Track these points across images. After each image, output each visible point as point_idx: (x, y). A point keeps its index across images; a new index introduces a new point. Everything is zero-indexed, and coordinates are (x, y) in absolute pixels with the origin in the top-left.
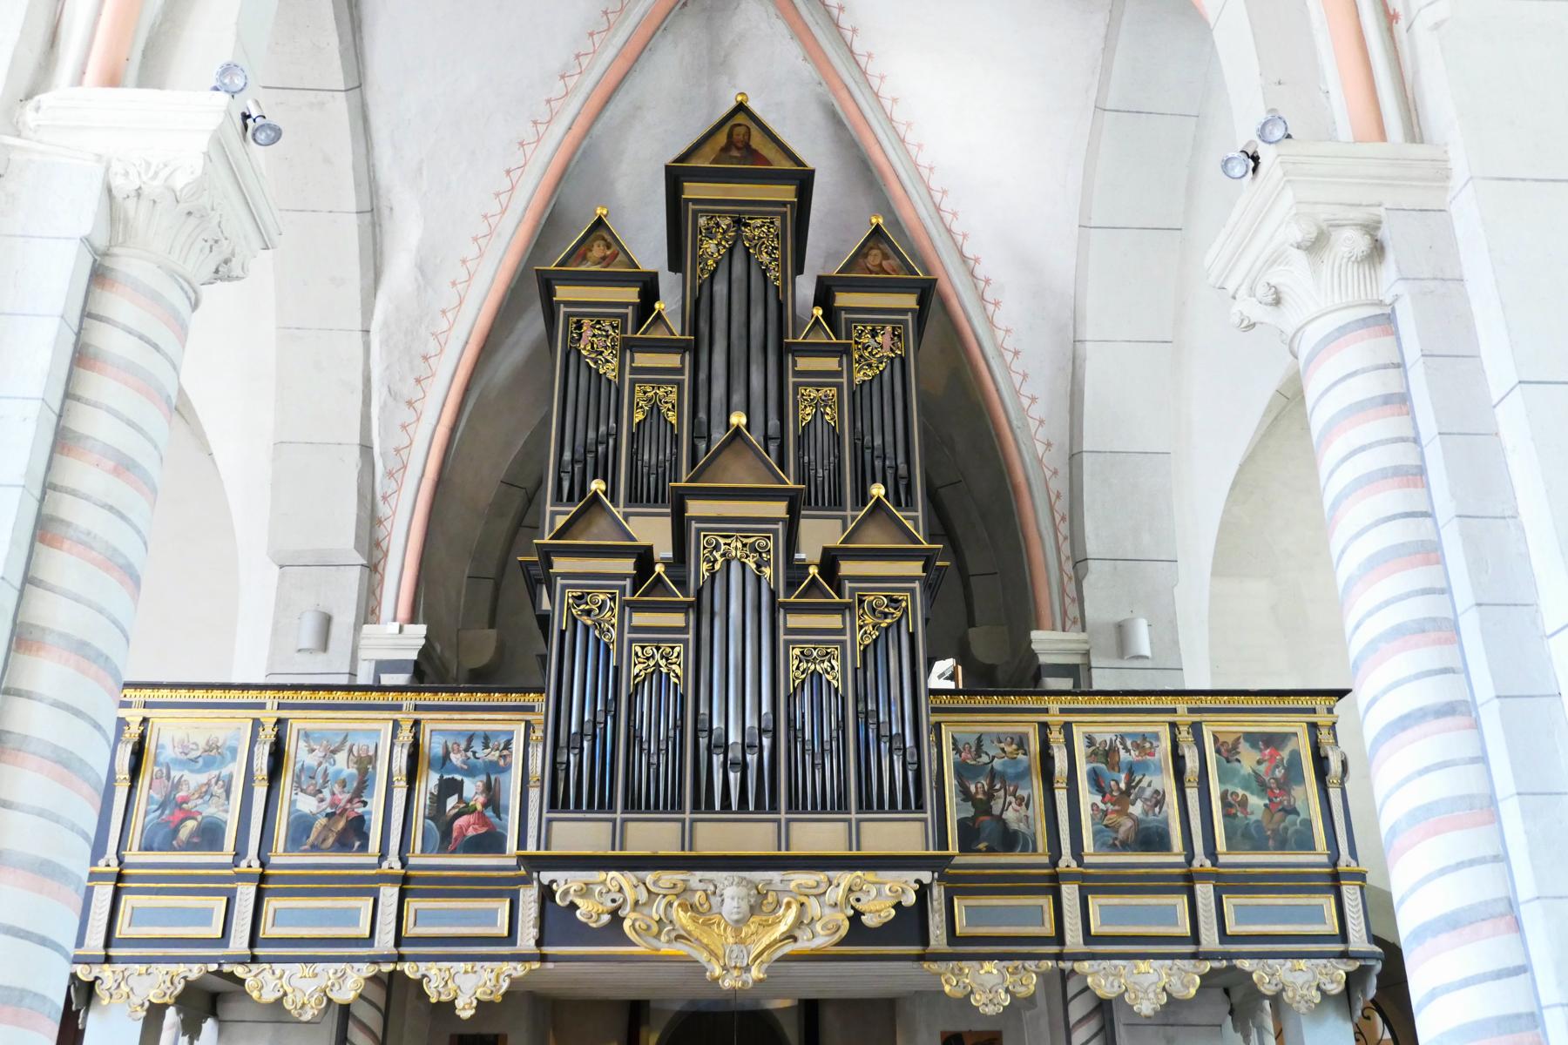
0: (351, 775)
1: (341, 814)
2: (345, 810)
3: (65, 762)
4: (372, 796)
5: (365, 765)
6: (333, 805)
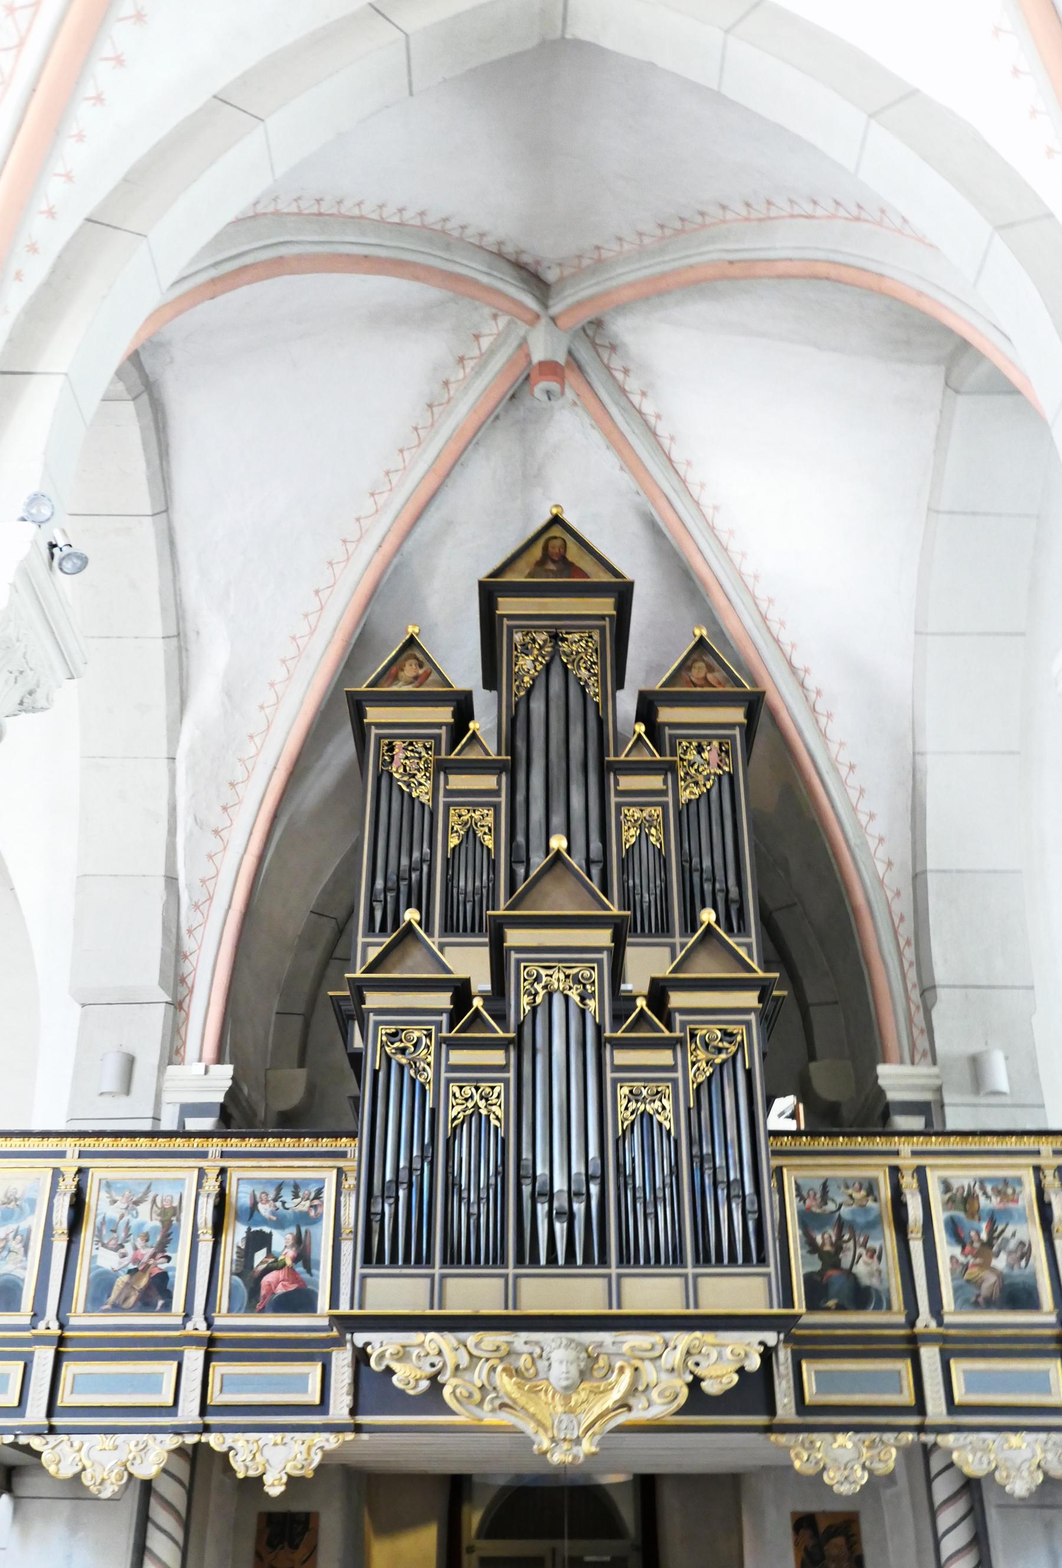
0: (155, 1228)
1: (144, 1270)
2: (147, 1266)
4: (175, 1251)
5: (169, 1217)
6: (135, 1260)
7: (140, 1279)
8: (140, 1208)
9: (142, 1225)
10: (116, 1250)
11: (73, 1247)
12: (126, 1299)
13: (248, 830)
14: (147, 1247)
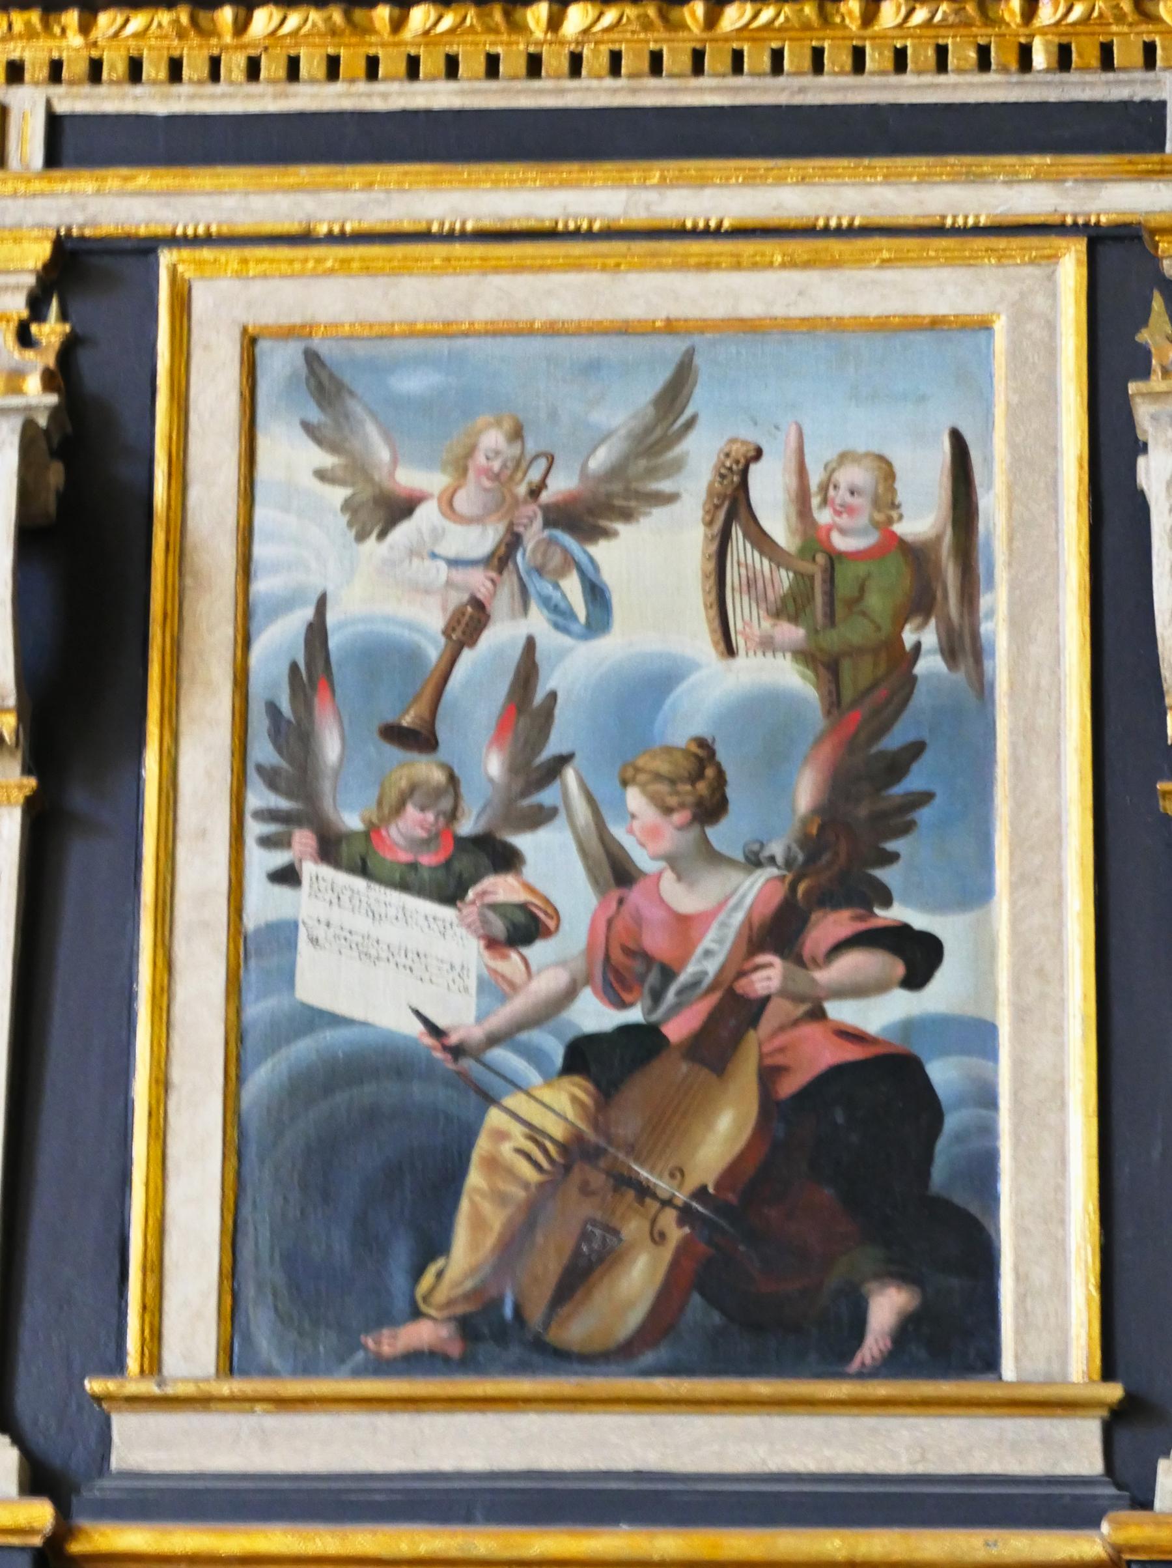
0: (760, 711)
1: (714, 1047)
2: (736, 1012)
3: (23, 49)
4: (973, 891)
5: (878, 623)
6: (624, 966)
7: (670, 1125)
8: (616, 556)
9: (656, 683)
10: (450, 891)
11: (81, 860)
12: (579, 1276)
13: (170, 1164)
14: (713, 857)
